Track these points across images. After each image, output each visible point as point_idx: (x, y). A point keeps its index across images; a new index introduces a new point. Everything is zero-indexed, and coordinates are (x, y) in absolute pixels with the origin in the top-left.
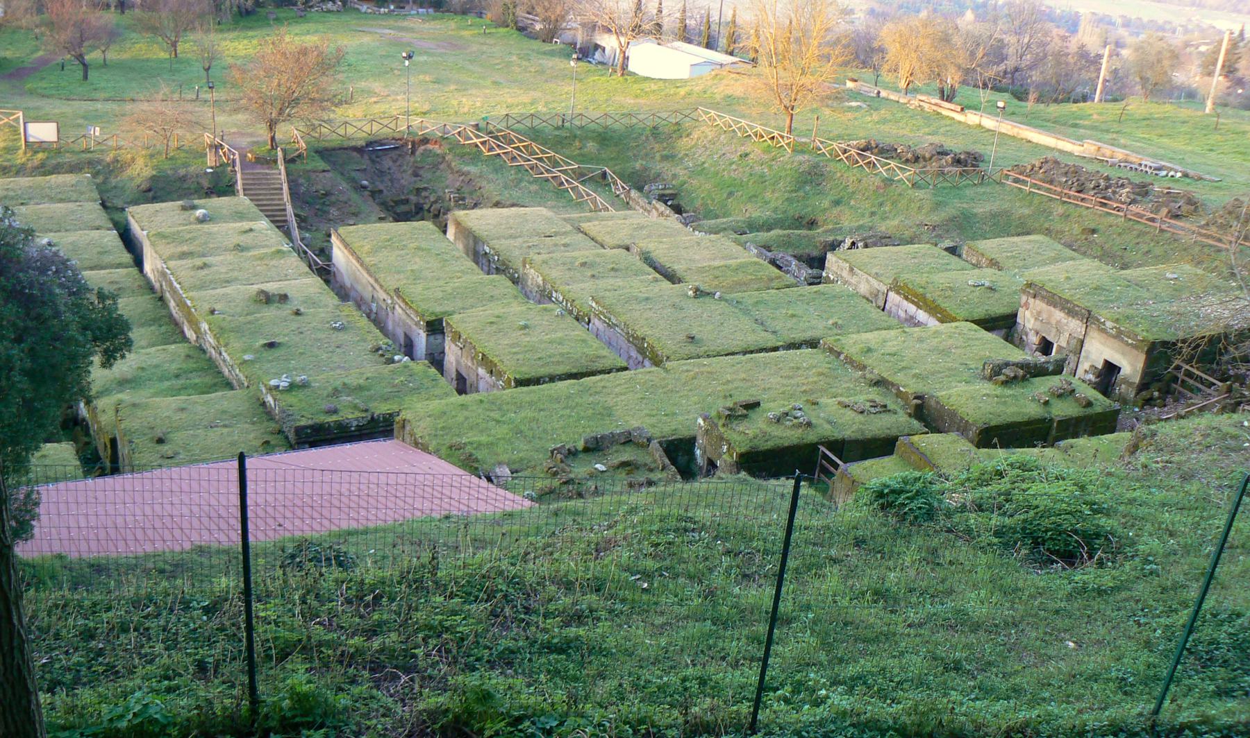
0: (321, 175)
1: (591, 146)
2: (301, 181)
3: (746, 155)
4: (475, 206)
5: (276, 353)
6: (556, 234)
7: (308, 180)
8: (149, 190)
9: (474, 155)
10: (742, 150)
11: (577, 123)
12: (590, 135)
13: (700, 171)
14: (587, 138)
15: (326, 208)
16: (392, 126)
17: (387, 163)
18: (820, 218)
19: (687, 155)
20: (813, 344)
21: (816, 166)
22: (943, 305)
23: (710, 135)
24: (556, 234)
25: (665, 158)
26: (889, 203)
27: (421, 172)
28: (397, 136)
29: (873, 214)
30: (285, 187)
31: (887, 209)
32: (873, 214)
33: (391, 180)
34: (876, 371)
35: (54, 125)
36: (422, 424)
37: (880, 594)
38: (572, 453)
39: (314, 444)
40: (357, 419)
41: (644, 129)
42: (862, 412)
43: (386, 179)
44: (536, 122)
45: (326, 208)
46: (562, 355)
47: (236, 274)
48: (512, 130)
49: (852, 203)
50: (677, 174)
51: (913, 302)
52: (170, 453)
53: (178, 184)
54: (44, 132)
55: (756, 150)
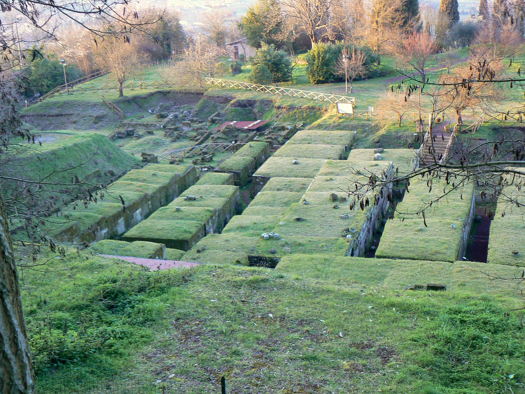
5: (299, 223)
8: (378, 142)
53: (396, 140)
54: (346, 108)
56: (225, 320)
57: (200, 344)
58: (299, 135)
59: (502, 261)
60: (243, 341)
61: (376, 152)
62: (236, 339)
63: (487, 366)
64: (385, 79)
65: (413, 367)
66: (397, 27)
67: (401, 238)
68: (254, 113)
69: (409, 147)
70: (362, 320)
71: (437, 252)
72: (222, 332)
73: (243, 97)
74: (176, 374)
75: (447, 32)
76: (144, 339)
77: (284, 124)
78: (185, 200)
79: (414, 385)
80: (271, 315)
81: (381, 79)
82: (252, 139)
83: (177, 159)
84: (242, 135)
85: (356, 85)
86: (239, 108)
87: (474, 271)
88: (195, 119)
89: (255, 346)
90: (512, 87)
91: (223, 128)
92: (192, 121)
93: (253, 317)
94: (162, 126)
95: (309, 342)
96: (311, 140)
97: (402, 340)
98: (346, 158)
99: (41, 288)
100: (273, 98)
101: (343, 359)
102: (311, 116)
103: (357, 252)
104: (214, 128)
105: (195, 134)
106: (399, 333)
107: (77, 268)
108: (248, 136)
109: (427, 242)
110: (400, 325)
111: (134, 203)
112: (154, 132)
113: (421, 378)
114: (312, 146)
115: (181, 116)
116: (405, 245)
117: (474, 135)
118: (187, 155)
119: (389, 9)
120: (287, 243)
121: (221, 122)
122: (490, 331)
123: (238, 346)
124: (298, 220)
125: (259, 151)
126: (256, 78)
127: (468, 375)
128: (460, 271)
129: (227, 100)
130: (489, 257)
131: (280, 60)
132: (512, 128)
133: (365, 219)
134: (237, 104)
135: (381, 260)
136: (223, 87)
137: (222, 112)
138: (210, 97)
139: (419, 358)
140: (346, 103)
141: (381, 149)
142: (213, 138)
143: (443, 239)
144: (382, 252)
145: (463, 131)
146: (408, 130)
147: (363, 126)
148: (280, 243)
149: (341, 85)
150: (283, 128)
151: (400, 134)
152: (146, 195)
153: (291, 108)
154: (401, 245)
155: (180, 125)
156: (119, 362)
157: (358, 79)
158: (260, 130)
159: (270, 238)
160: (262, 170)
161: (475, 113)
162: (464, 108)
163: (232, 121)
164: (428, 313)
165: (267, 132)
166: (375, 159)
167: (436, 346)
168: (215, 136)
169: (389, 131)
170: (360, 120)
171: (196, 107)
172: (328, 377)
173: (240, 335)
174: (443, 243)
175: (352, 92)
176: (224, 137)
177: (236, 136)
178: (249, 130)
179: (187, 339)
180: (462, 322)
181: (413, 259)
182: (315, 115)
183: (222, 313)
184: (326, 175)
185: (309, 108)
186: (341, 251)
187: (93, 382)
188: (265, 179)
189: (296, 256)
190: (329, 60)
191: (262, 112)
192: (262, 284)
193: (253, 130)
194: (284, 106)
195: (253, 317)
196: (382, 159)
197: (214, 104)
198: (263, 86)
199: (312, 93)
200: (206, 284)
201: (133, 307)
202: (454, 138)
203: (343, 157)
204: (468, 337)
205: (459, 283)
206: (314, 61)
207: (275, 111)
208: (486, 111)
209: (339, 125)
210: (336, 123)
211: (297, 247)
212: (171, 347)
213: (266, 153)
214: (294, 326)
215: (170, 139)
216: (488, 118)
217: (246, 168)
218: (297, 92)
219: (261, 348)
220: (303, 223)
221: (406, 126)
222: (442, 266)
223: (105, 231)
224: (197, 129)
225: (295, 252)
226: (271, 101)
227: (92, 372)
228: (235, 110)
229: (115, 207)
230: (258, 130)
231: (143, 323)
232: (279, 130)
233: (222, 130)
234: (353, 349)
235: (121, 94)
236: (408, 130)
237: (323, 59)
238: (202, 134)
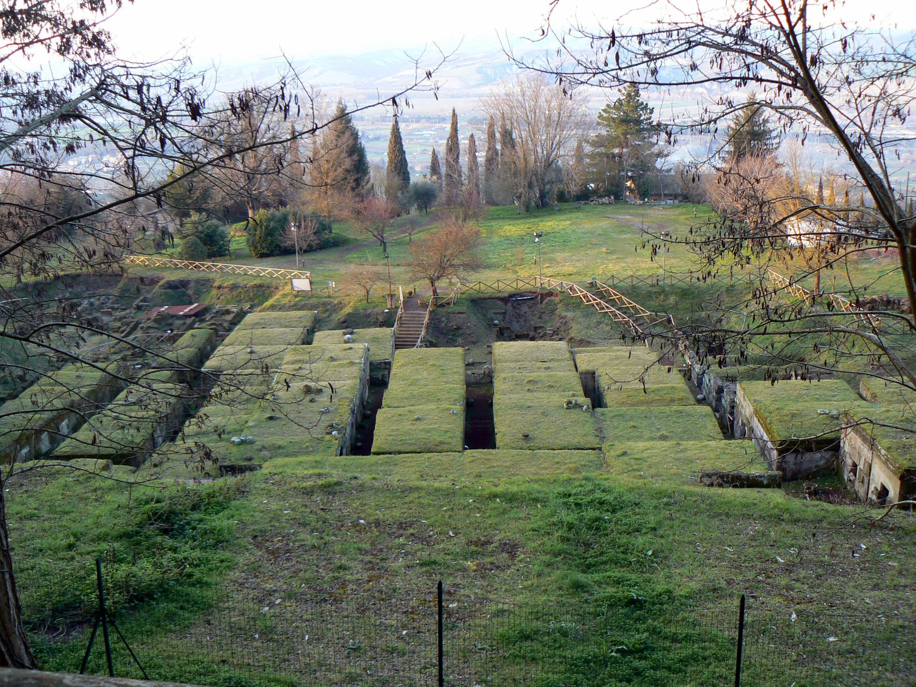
0: (457, 316)
2: (443, 319)
5: (273, 423)
7: (448, 319)
8: (345, 322)
9: (574, 303)
11: (668, 281)
14: (671, 294)
16: (532, 282)
17: (524, 308)
28: (533, 290)
33: (525, 321)
37: (702, 648)
43: (521, 320)
54: (302, 284)
56: (312, 531)
57: (294, 562)
58: (249, 318)
59: (513, 445)
60: (344, 553)
61: (345, 334)
62: (334, 552)
63: (619, 547)
64: (340, 249)
65: (547, 558)
66: (349, 188)
67: (398, 430)
68: (189, 296)
69: (380, 326)
70: (468, 516)
71: (441, 443)
72: (314, 546)
74: (284, 599)
75: (399, 194)
76: (225, 564)
77: (229, 307)
79: (553, 578)
80: (362, 521)
81: (334, 250)
82: (191, 327)
83: (101, 356)
84: (178, 322)
85: (307, 258)
86: (169, 290)
87: (488, 460)
88: (116, 306)
89: (361, 557)
91: (154, 315)
92: (113, 308)
93: (342, 526)
95: (420, 546)
96: (265, 323)
97: (522, 531)
98: (310, 343)
99: (66, 517)
100: (211, 276)
101: (466, 559)
103: (344, 451)
104: (141, 316)
105: (118, 324)
106: (513, 525)
107: (100, 488)
108: (184, 324)
109: (428, 432)
110: (512, 516)
113: (558, 568)
114: (268, 331)
115: (97, 303)
116: (403, 438)
117: (452, 309)
118: (113, 350)
119: (339, 170)
120: (264, 447)
121: (149, 308)
122: (608, 511)
123: (340, 559)
125: (203, 341)
126: (187, 253)
127: (604, 558)
128: (473, 461)
129: (153, 282)
130: (498, 443)
131: (214, 231)
132: (490, 298)
133: (349, 411)
135: (381, 456)
136: (146, 266)
137: (149, 296)
139: (548, 547)
140: (300, 278)
141: (349, 330)
142: (142, 328)
143: (445, 427)
144: (378, 448)
145: (440, 304)
146: (377, 306)
147: (324, 304)
148: (256, 448)
149: (290, 258)
150: (228, 312)
151: (368, 312)
153: (234, 287)
154: (399, 438)
155: (98, 315)
156: (209, 593)
157: (309, 250)
158: (199, 315)
159: (242, 442)
160: (211, 364)
161: (451, 283)
162: (438, 278)
163: (162, 306)
164: (536, 500)
165: (208, 317)
166: (346, 342)
167: (560, 533)
169: (356, 308)
170: (320, 297)
171: (115, 291)
172: (458, 581)
173: (338, 547)
174: (446, 432)
175: (304, 266)
177: (171, 324)
178: (186, 316)
179: (276, 558)
180: (578, 505)
181: (416, 452)
182: (263, 294)
183: (304, 525)
184: (293, 363)
185: (256, 286)
186: (330, 450)
187: (189, 619)
188: (216, 374)
189: (280, 461)
190: (273, 229)
191: (198, 294)
192: (338, 488)
193: (190, 316)
194: (225, 285)
195: (342, 526)
196: (354, 341)
198: (197, 263)
199: (257, 268)
200: (269, 494)
201: (194, 528)
202: (431, 312)
203: (307, 340)
204: (589, 520)
205: (475, 474)
207: (214, 292)
208: (464, 281)
209: (295, 305)
210: (293, 303)
211: (277, 450)
212: (262, 570)
213: (211, 342)
214: (394, 530)
216: (464, 289)
217: (190, 362)
218: (239, 268)
219: (368, 558)
220: (277, 421)
221: (374, 302)
222: (451, 458)
223: (25, 451)
224: (120, 319)
225: (275, 456)
226: (208, 280)
227: (182, 608)
230: (197, 315)
231: (215, 546)
232: (223, 314)
233: (153, 318)
234: (473, 548)
235: (19, 281)
236: (377, 306)
237: (266, 228)
238: (128, 324)
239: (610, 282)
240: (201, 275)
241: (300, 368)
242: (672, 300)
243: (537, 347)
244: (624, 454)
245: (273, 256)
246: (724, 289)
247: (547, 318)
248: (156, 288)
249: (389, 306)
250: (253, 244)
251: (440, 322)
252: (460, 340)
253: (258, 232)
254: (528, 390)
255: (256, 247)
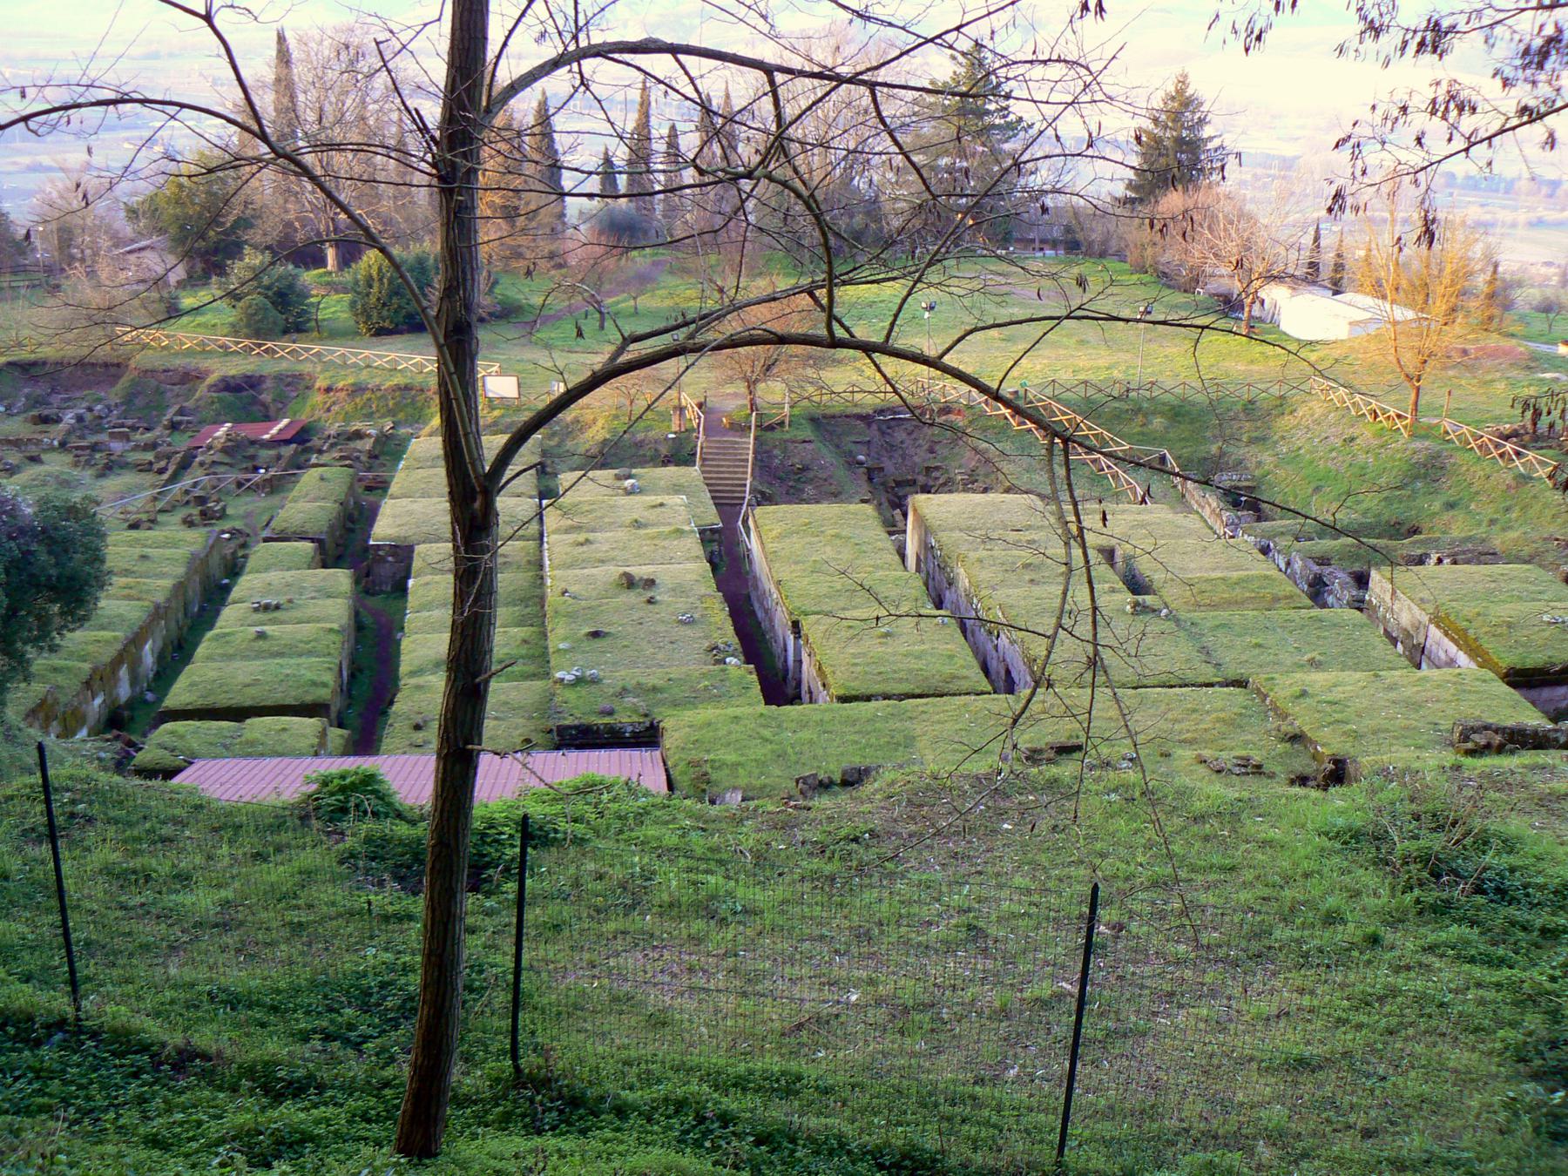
0: (801, 446)
1: (1158, 422)
2: (776, 452)
3: (1352, 439)
4: (985, 491)
5: (598, 644)
6: (1029, 528)
7: (785, 451)
10: (1350, 432)
12: (1160, 408)
13: (1294, 458)
14: (1154, 413)
15: (800, 486)
17: (900, 435)
18: (1425, 526)
19: (1283, 438)
20: (1240, 683)
21: (1437, 456)
22: (1485, 645)
23: (1318, 412)
24: (1029, 528)
25: (1253, 441)
26: (1517, 508)
27: (937, 448)
29: (1492, 522)
30: (750, 457)
31: (1514, 515)
32: (1492, 522)
33: (903, 457)
34: (1297, 723)
35: (514, 379)
36: (676, 735)
38: (825, 786)
39: (581, 747)
40: (632, 724)
41: (1234, 403)
42: (1219, 772)
44: (1091, 392)
45: (800, 486)
46: (910, 671)
47: (616, 553)
48: (1058, 401)
49: (1473, 506)
50: (1261, 462)
51: (1453, 640)
52: (420, 742)
53: (633, 450)
55: (1366, 433)
68: (263, 405)
73: (222, 369)
78: (256, 610)
84: (266, 454)
86: (226, 394)
90: (580, 334)
94: (56, 443)
100: (306, 368)
102: (406, 406)
108: (279, 457)
111: (141, 628)
112: (43, 457)
117: (788, 433)
124: (596, 635)
129: (189, 378)
134: (221, 386)
137: (189, 404)
138: (149, 372)
142: (202, 464)
150: (358, 435)
152: (157, 607)
153: (357, 389)
168: (208, 458)
176: (227, 460)
185: (398, 388)
193: (287, 442)
194: (341, 385)
197: (158, 388)
198: (269, 344)
202: (756, 438)
206: (371, 287)
207: (317, 399)
215: (90, 472)
218: (356, 355)
228: (220, 400)
229: (107, 642)
239: (1049, 391)
240: (284, 366)
241: (587, 541)
242: (1158, 422)
243: (993, 504)
244: (1304, 694)
245: (401, 332)
246: (1239, 407)
247: (946, 452)
248: (202, 390)
249: (675, 428)
250: (364, 311)
251: (772, 457)
252: (809, 490)
253: (375, 290)
254: (1032, 581)
255: (369, 317)
